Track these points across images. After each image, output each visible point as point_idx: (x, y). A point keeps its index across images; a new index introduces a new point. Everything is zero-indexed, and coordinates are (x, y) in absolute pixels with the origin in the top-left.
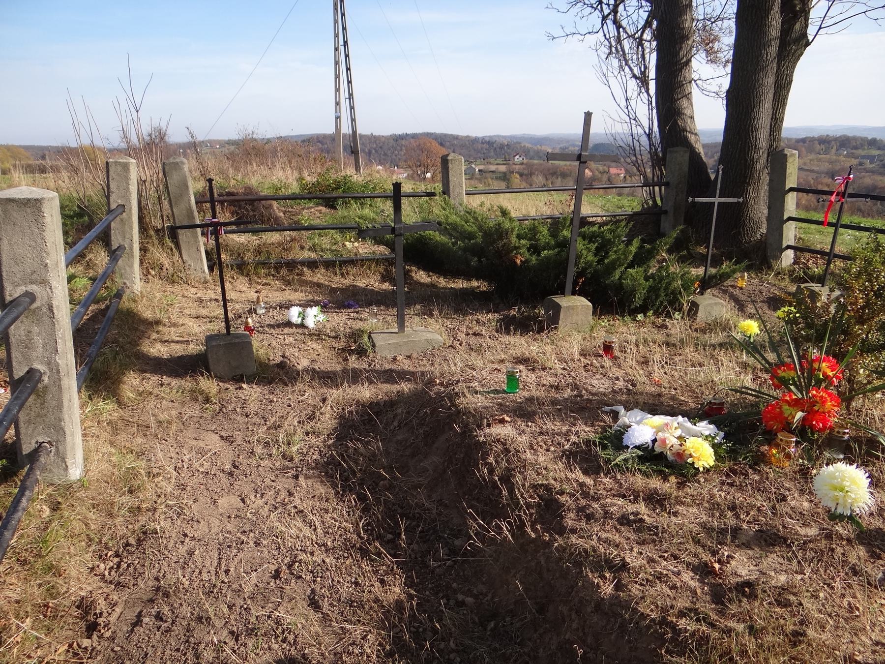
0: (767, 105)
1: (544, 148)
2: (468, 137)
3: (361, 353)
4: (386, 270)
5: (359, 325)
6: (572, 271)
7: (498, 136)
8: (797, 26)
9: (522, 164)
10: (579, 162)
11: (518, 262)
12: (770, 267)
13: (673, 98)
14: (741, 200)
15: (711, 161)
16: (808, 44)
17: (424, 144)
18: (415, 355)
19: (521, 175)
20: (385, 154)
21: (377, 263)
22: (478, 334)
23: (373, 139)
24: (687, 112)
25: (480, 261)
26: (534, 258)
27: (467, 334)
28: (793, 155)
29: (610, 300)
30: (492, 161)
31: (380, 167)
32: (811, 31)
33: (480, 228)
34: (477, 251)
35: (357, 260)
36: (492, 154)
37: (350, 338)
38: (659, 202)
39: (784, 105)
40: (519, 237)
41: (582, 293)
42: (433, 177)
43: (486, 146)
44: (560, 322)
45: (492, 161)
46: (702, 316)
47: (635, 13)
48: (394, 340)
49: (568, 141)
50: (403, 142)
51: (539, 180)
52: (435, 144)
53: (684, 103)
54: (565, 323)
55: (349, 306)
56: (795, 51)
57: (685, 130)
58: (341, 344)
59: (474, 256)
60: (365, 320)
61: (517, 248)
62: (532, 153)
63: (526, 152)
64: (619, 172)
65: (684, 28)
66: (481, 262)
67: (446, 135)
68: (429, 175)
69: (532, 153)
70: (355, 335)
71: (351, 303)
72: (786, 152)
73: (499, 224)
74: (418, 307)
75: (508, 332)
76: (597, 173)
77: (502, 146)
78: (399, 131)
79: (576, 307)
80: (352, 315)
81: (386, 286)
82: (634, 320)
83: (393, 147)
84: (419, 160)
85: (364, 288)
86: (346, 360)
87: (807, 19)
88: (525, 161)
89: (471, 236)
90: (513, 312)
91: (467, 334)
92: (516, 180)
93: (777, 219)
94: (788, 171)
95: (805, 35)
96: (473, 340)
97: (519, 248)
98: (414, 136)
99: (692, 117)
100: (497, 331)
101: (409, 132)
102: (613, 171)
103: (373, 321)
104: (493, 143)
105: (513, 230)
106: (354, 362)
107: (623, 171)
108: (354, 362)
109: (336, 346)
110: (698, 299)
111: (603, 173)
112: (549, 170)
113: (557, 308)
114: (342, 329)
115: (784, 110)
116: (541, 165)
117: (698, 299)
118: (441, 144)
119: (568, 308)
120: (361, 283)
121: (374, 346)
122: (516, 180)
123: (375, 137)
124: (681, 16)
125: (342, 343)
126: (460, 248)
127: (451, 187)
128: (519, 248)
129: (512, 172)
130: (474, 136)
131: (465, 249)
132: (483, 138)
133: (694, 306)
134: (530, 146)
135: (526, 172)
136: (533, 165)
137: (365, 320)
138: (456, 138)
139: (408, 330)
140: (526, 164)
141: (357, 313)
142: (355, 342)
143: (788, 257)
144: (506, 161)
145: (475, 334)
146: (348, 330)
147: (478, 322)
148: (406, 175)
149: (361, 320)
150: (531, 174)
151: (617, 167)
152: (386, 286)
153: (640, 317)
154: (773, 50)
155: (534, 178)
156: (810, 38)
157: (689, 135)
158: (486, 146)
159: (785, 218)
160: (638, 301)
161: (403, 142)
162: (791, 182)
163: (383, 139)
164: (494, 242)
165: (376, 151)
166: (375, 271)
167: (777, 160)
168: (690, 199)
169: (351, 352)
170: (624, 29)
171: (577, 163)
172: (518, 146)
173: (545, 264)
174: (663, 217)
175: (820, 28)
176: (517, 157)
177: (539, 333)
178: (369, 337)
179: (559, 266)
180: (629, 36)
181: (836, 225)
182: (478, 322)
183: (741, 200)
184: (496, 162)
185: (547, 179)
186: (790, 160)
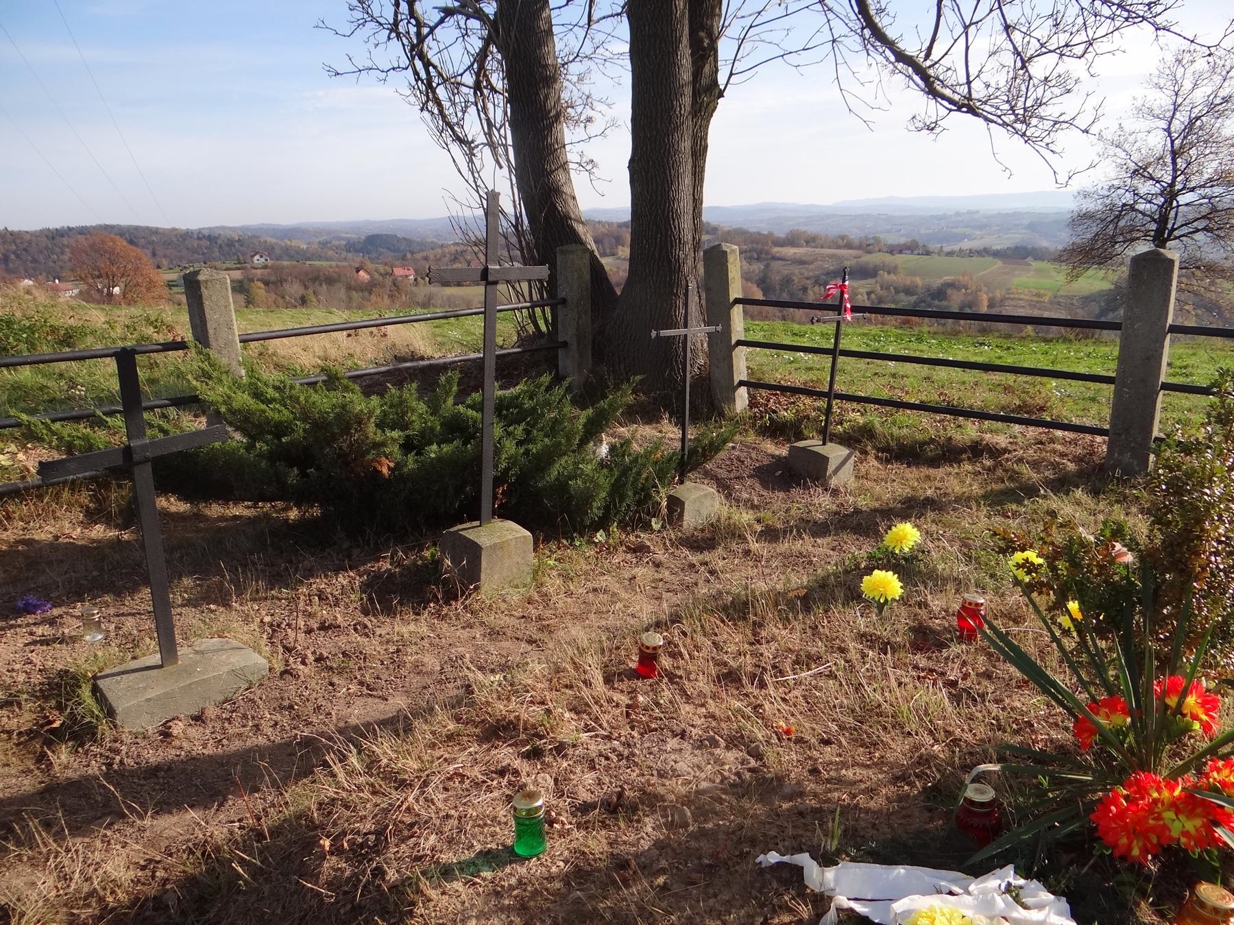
0: (687, 180)
1: (294, 243)
2: (174, 229)
3: (80, 734)
4: (94, 498)
5: (61, 659)
6: (489, 474)
7: (223, 228)
8: (707, 69)
9: (265, 267)
10: (368, 266)
11: (385, 471)
12: (721, 414)
13: (544, 170)
14: (719, 328)
15: (616, 265)
16: (721, 95)
17: (103, 242)
18: (211, 712)
19: (266, 283)
20: (34, 261)
21: (73, 490)
22: (330, 627)
23: (9, 238)
24: (565, 189)
25: (303, 474)
26: (411, 457)
27: (309, 631)
28: (733, 251)
29: (552, 515)
30: (218, 264)
31: (28, 282)
32: (722, 79)
33: (305, 417)
34: (300, 456)
35: (27, 489)
36: (216, 254)
37: (47, 699)
38: (544, 328)
39: (702, 180)
40: (381, 425)
41: (504, 513)
42: (124, 294)
43: (205, 243)
44: (483, 576)
45: (218, 264)
46: (691, 519)
47: (456, 46)
48: (157, 686)
49: (329, 232)
50: (65, 241)
51: (294, 289)
52: (122, 243)
53: (561, 176)
54: (492, 580)
55: (29, 610)
56: (708, 104)
57: (568, 217)
58: (24, 719)
59: (291, 466)
60: (73, 639)
61: (378, 446)
62: (278, 251)
63: (269, 250)
64: (407, 272)
65: (547, 65)
66: (307, 476)
67: (137, 228)
68: (117, 290)
69: (278, 251)
70: (60, 687)
71: (32, 599)
72: (725, 249)
73: (344, 407)
74: (187, 582)
75: (390, 611)
76: (377, 276)
77: (230, 243)
78: (55, 223)
79: (503, 540)
80: (39, 631)
81: (99, 532)
82: (590, 542)
83: (47, 248)
84: (96, 268)
85: (51, 544)
86: (41, 758)
87: (716, 60)
88: (270, 262)
89: (280, 429)
90: (386, 566)
91: (309, 631)
92: (259, 290)
93: (722, 346)
94: (730, 276)
95: (715, 83)
96: (327, 645)
97: (383, 444)
98: (83, 231)
99: (574, 198)
100: (366, 613)
101: (72, 225)
102: (398, 272)
103: (89, 639)
104: (216, 238)
105: (371, 413)
106: (65, 761)
107: (412, 271)
108: (65, 761)
109: (13, 724)
110: (681, 491)
111: (383, 275)
112: (307, 274)
113: (474, 551)
114: (22, 678)
115: (702, 187)
116: (294, 267)
117: (681, 491)
118: (131, 242)
119: (494, 547)
120: (43, 533)
121: (111, 713)
122: (259, 290)
123: (12, 234)
124: (540, 47)
125: (28, 716)
126: (261, 455)
127: (211, 332)
128: (383, 444)
129: (252, 280)
130: (184, 228)
131: (272, 457)
132: (200, 231)
133: (676, 504)
134: (274, 241)
135: (273, 278)
136: (283, 268)
137: (73, 639)
138: (155, 231)
139: (183, 651)
140: (272, 268)
141: (52, 622)
142: (60, 708)
143: (742, 397)
144: (241, 264)
145: (323, 627)
146: (37, 678)
147: (322, 596)
148: (76, 291)
149: (62, 640)
150: (281, 281)
151: (403, 266)
152: (99, 532)
153: (600, 536)
154: (687, 100)
155: (286, 286)
156: (722, 87)
157: (575, 225)
158: (205, 243)
159: (733, 342)
160: (596, 509)
161: (65, 241)
162: (735, 292)
163: (28, 237)
164: (334, 438)
165: (18, 256)
166: (70, 504)
167: (716, 260)
168: (654, 334)
169: (57, 736)
170: (435, 67)
171: (480, 290)
172: (255, 241)
173: (432, 472)
174: (561, 352)
175: (731, 74)
176: (257, 257)
177: (447, 603)
178: (95, 690)
179: (465, 471)
180: (445, 81)
181: (834, 352)
182: (322, 596)
183: (719, 328)
184: (225, 266)
185: (306, 288)
186: (731, 258)
